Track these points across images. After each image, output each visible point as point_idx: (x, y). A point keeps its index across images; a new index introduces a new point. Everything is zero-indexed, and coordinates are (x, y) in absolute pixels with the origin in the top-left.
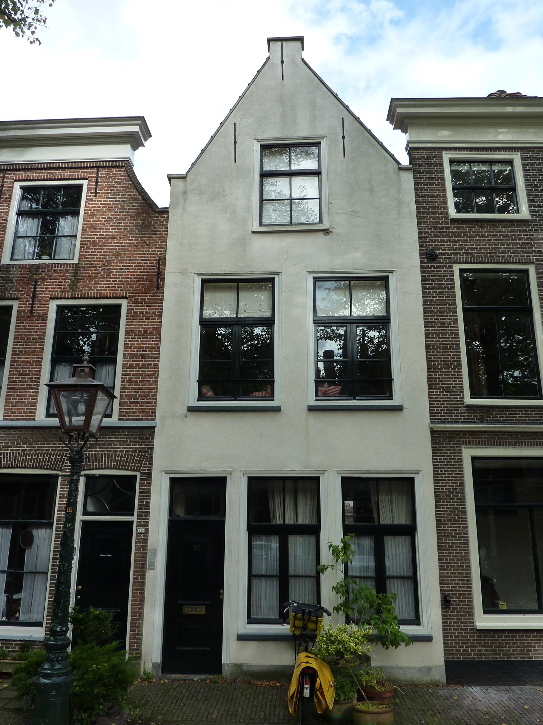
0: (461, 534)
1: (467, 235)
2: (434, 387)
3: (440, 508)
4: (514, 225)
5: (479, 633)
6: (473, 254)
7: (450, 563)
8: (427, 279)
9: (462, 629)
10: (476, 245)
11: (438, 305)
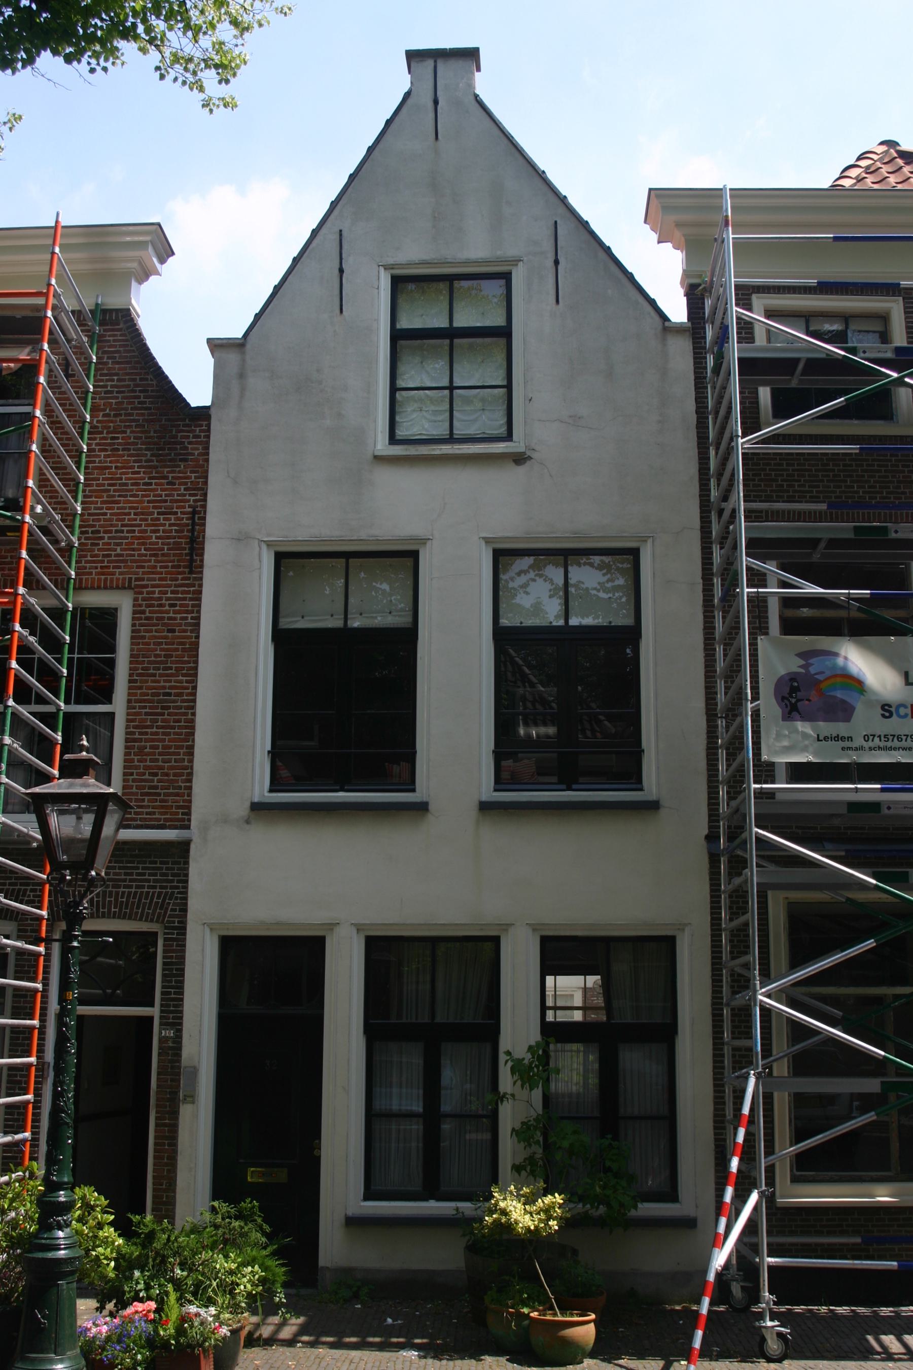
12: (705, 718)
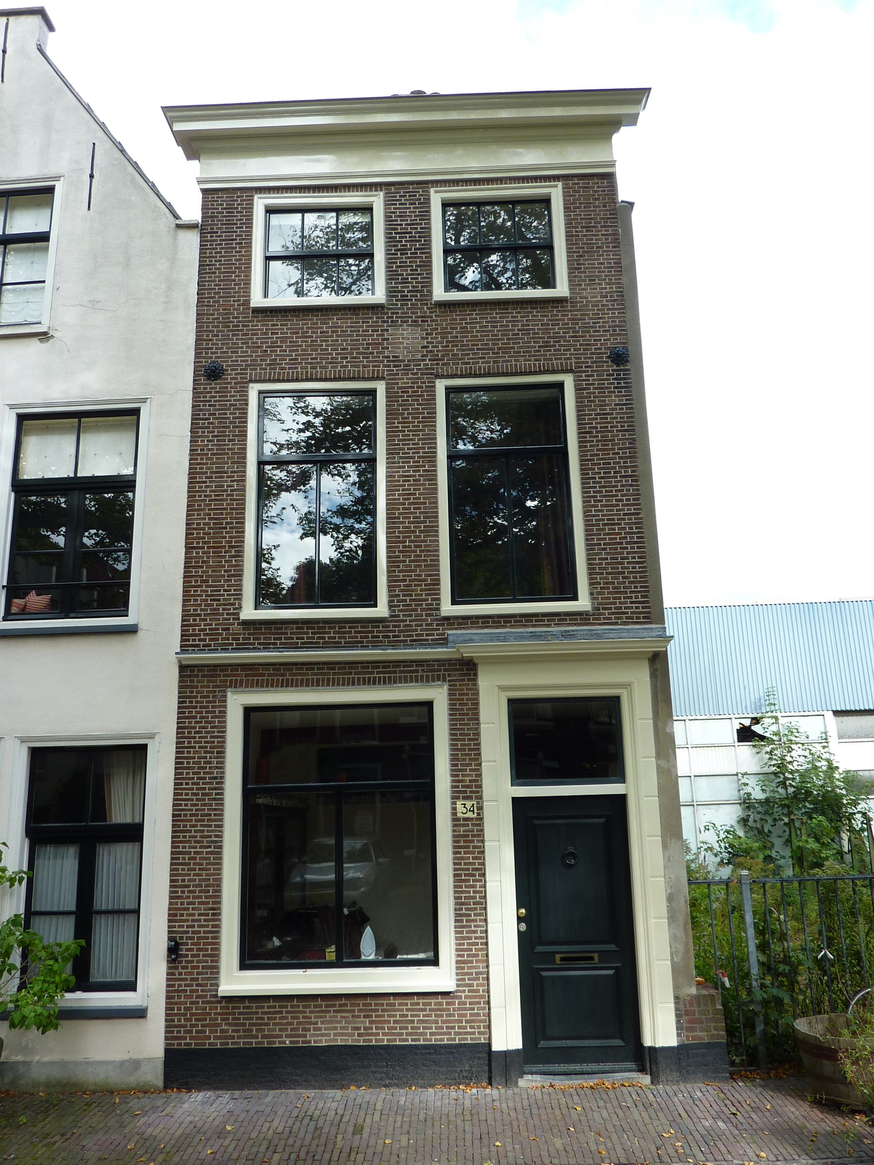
0: (210, 836)
1: (277, 333)
2: (192, 593)
3: (181, 794)
4: (358, 314)
5: (226, 1002)
6: (284, 366)
7: (188, 886)
8: (201, 410)
9: (198, 997)
10: (289, 351)
11: (214, 454)
12: (184, 550)
